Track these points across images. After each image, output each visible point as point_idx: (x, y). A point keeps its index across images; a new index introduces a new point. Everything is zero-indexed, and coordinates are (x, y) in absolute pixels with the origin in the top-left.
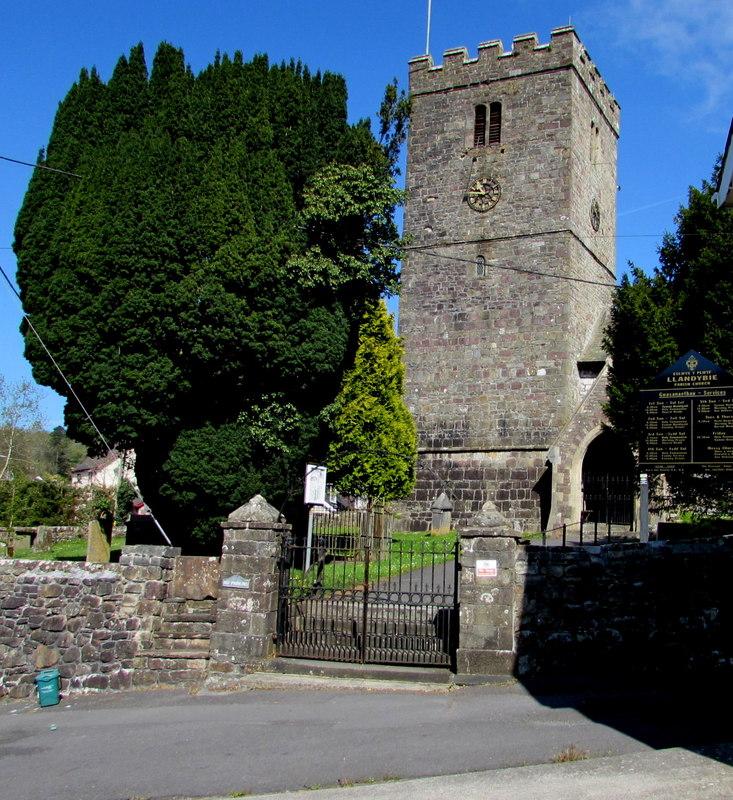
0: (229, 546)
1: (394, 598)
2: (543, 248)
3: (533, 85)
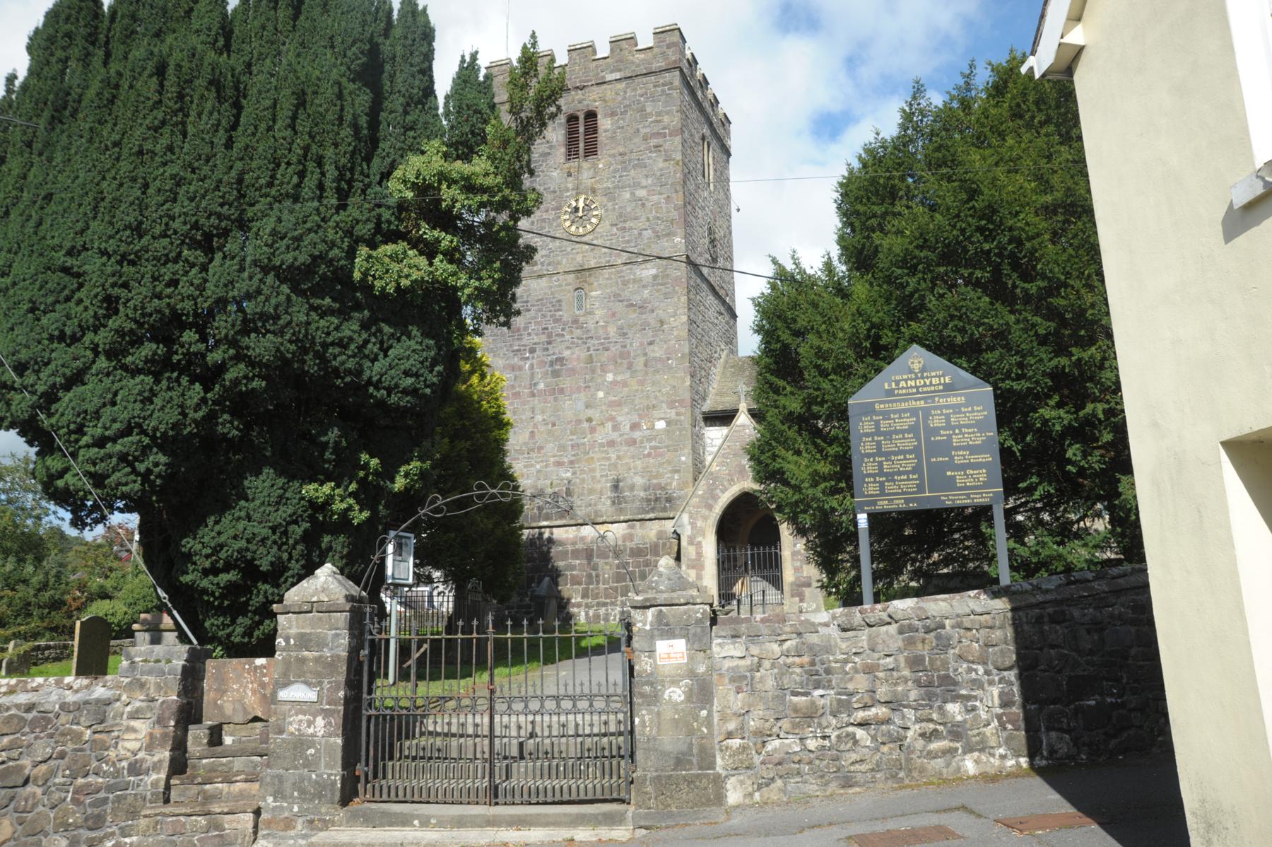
0: (287, 640)
1: (550, 705)
2: (655, 277)
3: (635, 90)
